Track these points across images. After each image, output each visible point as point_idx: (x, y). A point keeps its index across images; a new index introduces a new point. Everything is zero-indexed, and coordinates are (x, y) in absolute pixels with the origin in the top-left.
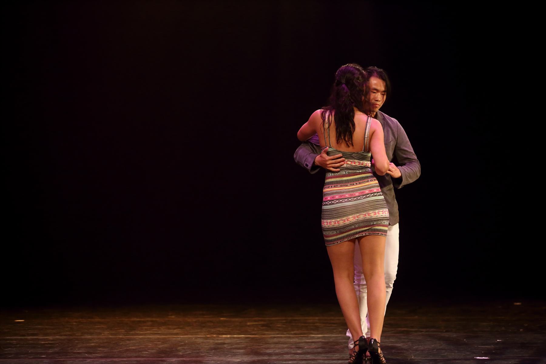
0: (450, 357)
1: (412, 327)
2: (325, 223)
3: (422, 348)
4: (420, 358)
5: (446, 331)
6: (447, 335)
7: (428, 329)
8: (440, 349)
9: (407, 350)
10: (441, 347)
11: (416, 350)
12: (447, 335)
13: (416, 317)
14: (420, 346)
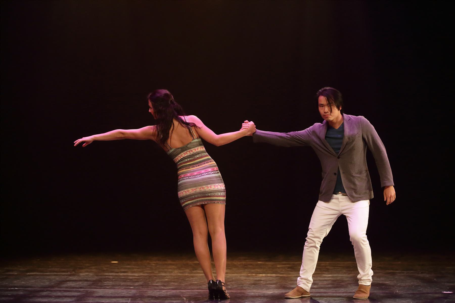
0: (425, 291)
1: (397, 270)
2: (184, 193)
3: (404, 285)
4: (402, 292)
5: (421, 273)
6: (421, 275)
7: (408, 272)
8: (417, 286)
9: (393, 286)
10: (417, 284)
11: (400, 286)
12: (421, 275)
13: (400, 262)
14: (401, 282)
